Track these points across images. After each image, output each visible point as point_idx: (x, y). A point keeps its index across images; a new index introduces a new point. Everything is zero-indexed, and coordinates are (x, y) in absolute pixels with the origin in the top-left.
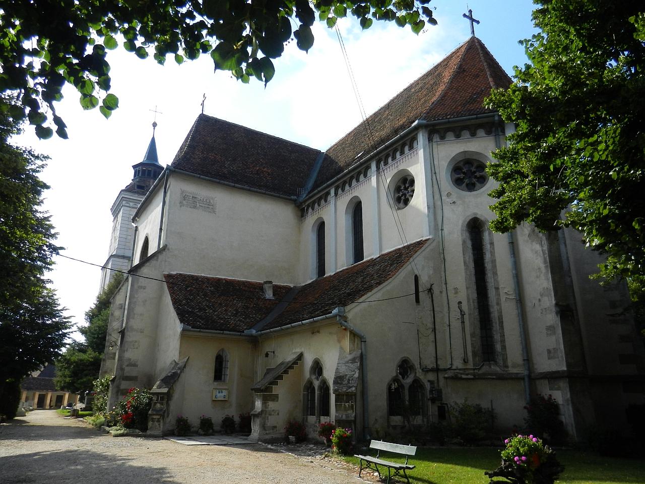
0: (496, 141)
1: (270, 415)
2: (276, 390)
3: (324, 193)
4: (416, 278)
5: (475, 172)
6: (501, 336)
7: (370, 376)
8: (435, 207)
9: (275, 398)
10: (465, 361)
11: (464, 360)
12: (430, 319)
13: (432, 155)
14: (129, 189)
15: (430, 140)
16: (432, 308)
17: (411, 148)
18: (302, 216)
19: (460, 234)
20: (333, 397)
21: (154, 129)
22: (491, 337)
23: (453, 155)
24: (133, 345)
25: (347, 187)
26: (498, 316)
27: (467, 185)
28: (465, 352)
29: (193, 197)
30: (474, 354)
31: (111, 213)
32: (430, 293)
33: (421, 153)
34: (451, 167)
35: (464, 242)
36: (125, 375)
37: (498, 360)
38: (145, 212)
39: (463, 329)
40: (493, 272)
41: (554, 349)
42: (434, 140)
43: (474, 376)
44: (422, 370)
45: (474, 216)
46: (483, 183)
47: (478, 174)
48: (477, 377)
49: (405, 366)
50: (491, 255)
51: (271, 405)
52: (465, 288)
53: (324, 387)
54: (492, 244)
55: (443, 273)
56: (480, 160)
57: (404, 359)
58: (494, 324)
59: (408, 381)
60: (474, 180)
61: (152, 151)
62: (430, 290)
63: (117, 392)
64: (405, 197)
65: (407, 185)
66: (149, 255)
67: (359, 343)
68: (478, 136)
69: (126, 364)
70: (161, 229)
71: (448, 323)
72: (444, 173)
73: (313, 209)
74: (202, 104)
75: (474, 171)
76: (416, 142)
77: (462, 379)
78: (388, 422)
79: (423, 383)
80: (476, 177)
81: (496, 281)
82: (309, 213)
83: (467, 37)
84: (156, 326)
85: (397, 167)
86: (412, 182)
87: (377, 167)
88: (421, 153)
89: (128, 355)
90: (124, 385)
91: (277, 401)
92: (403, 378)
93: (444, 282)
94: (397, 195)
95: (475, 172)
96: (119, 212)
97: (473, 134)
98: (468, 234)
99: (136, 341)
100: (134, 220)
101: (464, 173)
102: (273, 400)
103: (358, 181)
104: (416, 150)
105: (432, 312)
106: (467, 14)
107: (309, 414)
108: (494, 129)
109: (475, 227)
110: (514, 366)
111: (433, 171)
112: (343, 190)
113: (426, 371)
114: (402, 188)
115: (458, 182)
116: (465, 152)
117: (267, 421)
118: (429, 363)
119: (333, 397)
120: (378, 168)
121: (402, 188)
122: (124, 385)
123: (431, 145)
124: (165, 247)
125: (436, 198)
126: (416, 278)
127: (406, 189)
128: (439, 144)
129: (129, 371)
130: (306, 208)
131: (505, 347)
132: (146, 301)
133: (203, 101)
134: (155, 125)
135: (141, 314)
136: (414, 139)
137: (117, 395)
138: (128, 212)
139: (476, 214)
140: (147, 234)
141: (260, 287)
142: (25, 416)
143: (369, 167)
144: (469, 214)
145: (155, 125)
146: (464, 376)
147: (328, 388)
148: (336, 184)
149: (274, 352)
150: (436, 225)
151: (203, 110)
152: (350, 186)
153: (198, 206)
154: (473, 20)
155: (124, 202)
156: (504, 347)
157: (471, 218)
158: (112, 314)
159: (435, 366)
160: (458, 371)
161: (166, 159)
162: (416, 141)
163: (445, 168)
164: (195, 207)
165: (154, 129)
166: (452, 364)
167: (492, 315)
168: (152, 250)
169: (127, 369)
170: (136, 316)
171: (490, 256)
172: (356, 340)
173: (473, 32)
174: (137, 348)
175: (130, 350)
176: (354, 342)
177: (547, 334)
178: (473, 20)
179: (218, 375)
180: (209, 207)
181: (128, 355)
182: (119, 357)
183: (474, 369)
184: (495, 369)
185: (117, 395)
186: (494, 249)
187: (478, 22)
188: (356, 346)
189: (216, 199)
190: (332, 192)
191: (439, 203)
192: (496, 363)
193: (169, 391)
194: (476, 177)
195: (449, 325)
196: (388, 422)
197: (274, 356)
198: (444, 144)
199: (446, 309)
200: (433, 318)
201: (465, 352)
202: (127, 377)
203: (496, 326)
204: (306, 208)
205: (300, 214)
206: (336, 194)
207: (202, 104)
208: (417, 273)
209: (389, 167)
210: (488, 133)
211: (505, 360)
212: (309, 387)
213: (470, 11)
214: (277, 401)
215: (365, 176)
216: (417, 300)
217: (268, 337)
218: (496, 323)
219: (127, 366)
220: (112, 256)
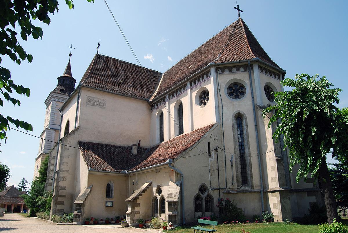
0: (249, 74)
1: (136, 213)
2: (138, 201)
3: (163, 97)
4: (209, 144)
5: (239, 89)
6: (250, 172)
7: (185, 193)
8: (219, 107)
9: (138, 205)
10: (233, 184)
11: (232, 184)
12: (216, 164)
13: (217, 80)
14: (54, 91)
15: (217, 72)
16: (217, 159)
17: (207, 76)
18: (152, 109)
19: (231, 121)
20: (167, 204)
21: (70, 57)
22: (246, 172)
23: (228, 80)
24: (63, 179)
25: (175, 95)
26: (249, 162)
27: (235, 96)
28: (233, 181)
29: (93, 100)
30: (238, 181)
31: (45, 104)
32: (216, 151)
33: (212, 79)
34: (227, 87)
35: (233, 125)
36: (59, 194)
37: (249, 184)
38: (67, 107)
39: (232, 169)
40: (247, 140)
41: (274, 177)
42: (219, 73)
43: (237, 192)
44: (212, 189)
45: (238, 112)
46: (243, 95)
47: (240, 90)
48: (238, 192)
49: (203, 189)
50: (246, 132)
51: (137, 209)
52: (234, 148)
53: (163, 199)
54: (247, 126)
55: (223, 141)
56: (241, 83)
57: (204, 184)
58: (247, 166)
59: (204, 196)
60: (239, 93)
61: (69, 69)
62: (216, 149)
63: (56, 204)
64: (204, 101)
65: (205, 95)
66: (69, 132)
67: (180, 177)
68: (240, 71)
69: (60, 188)
70: (76, 117)
71: (225, 166)
72: (224, 90)
73: (157, 106)
74: (98, 48)
75: (239, 89)
76: (209, 73)
77: (231, 193)
78: (194, 215)
79: (212, 196)
80: (239, 92)
81: (249, 144)
82: (155, 108)
83: (236, 19)
84: (76, 169)
85: (200, 85)
86: (208, 94)
87: (190, 85)
88: (212, 79)
89: (61, 184)
90: (59, 199)
91: (139, 207)
92: (202, 194)
93: (223, 145)
94: (200, 100)
95: (239, 89)
96: (50, 104)
97: (238, 70)
98: (235, 121)
99: (65, 177)
100: (60, 111)
101: (234, 90)
102: (137, 206)
103: (180, 91)
104: (210, 78)
105: (217, 161)
106: (236, 7)
107: (155, 212)
108: (248, 68)
109: (239, 118)
110: (256, 187)
111: (218, 89)
112: (173, 96)
113: (214, 189)
114: (203, 96)
115: (230, 95)
116: (234, 79)
117: (134, 217)
118: (216, 186)
119: (167, 204)
120: (191, 85)
121: (203, 96)
122: (59, 199)
123: (217, 74)
124: (78, 128)
125: (219, 102)
126: (209, 144)
127: (205, 97)
128: (221, 75)
129: (61, 192)
130: (153, 105)
131: (252, 177)
132: (69, 155)
133: (98, 47)
134: (70, 55)
135: (67, 163)
136: (209, 71)
137: (56, 204)
138: (55, 104)
139: (239, 111)
140: (68, 119)
141: (129, 149)
142: (4, 216)
143: (186, 85)
144: (236, 111)
145: (70, 55)
146: (232, 192)
147: (164, 200)
148: (169, 93)
149: (137, 182)
150: (220, 116)
151: (98, 52)
152: (176, 94)
153: (96, 104)
154: (239, 10)
155: (53, 98)
156: (252, 177)
157: (236, 113)
158: (50, 162)
159: (218, 188)
160: (229, 189)
161: (78, 75)
162: (210, 73)
163: (224, 87)
164: (94, 105)
165: (70, 57)
166: (226, 186)
167: (246, 162)
168: (72, 128)
169: (60, 191)
170: (64, 164)
171: (246, 132)
172: (178, 175)
173: (239, 16)
174: (65, 180)
175: (62, 181)
176: (177, 176)
177: (271, 170)
178: (239, 10)
179: (108, 194)
180: (102, 105)
181: (61, 184)
182: (56, 185)
183: (237, 188)
184: (247, 188)
185: (56, 204)
186: (248, 128)
187: (242, 11)
188: (178, 179)
189: (105, 100)
190: (167, 97)
191: (221, 105)
192: (248, 185)
193: (84, 202)
194: (239, 92)
195: (226, 167)
196: (194, 215)
197: (137, 184)
198: (224, 75)
199: (224, 159)
200: (217, 163)
201: (233, 181)
202: (61, 195)
203: (248, 167)
204: (153, 105)
205: (150, 108)
206: (169, 98)
207: (98, 48)
208: (191, 155)
209: (196, 85)
210: (245, 69)
211: (252, 183)
212: (156, 199)
213: (238, 6)
214: (139, 207)
215: (184, 89)
216: (210, 156)
217: (134, 174)
218: (248, 165)
219: (61, 190)
220: (46, 129)
